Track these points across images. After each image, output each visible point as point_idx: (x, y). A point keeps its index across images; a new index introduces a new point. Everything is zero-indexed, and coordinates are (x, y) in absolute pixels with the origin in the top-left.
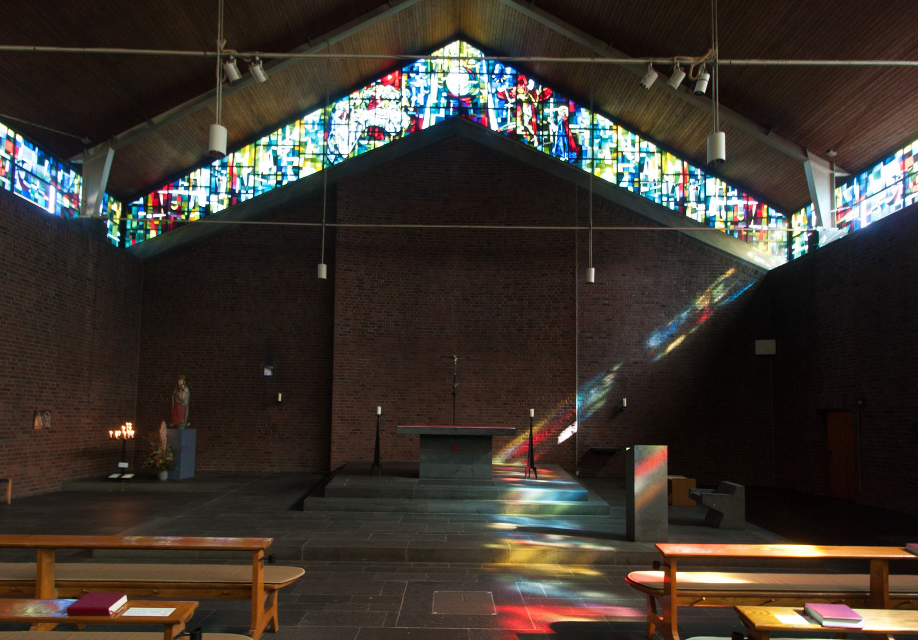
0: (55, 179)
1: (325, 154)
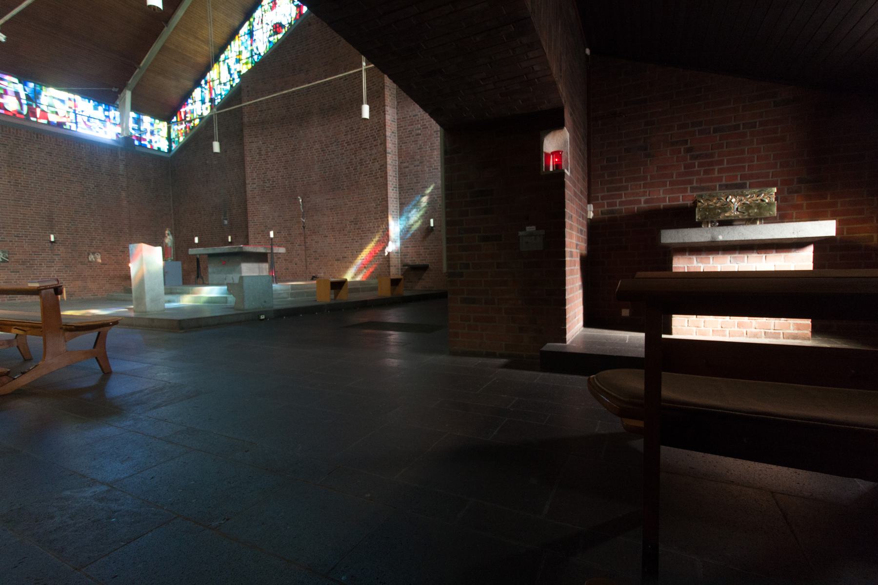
0: (108, 117)
1: (252, 56)
